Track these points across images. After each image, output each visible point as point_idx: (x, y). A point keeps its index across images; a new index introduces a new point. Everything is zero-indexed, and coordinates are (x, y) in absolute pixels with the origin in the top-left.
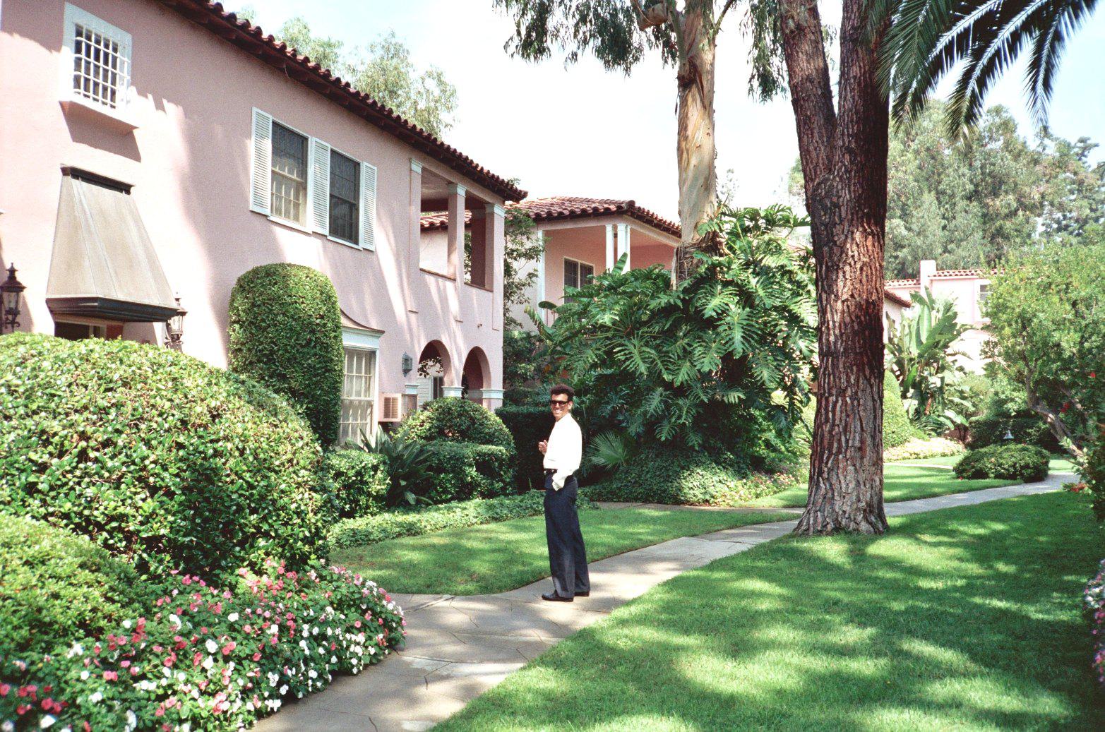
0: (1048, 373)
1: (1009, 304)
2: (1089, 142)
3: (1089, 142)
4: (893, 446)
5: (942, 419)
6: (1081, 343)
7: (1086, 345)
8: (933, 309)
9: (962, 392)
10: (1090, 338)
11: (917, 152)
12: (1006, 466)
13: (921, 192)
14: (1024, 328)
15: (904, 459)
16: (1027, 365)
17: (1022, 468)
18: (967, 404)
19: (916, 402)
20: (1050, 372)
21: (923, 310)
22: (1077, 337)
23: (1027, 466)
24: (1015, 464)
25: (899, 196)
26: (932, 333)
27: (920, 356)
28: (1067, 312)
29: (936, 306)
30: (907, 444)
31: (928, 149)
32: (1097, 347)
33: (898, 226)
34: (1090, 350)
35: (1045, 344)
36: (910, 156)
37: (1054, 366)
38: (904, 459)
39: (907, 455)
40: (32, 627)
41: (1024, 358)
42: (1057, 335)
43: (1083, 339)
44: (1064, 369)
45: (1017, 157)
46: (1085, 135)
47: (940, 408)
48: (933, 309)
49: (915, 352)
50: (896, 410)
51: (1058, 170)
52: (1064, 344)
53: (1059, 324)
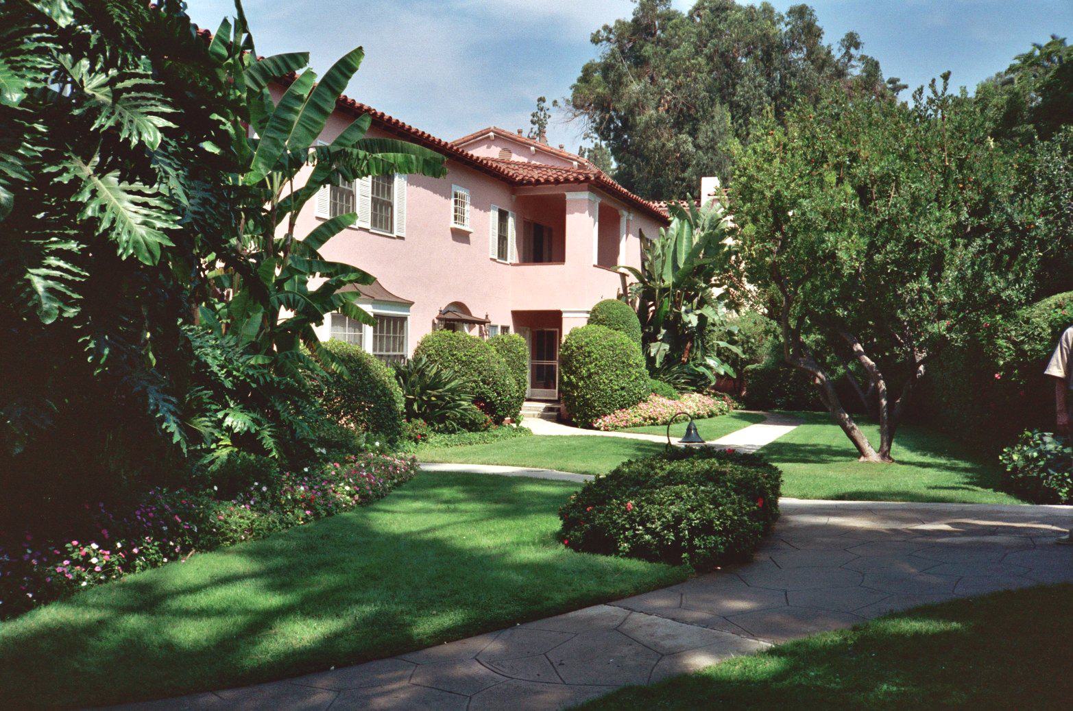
0: (816, 304)
1: (756, 186)
2: (898, 83)
3: (898, 83)
4: (621, 407)
5: (702, 369)
6: (869, 256)
7: (878, 258)
8: (697, 226)
9: (730, 333)
10: (884, 246)
11: (710, 58)
12: (657, 525)
13: (713, 105)
14: (777, 226)
15: (635, 425)
16: (783, 290)
17: (694, 531)
18: (737, 350)
19: (667, 347)
20: (820, 303)
21: (682, 226)
22: (863, 243)
23: (706, 528)
24: (678, 519)
25: (689, 108)
26: (693, 254)
27: (675, 285)
28: (845, 198)
29: (700, 223)
30: (642, 405)
31: (722, 55)
32: (895, 262)
33: (685, 142)
34: (884, 265)
35: (811, 252)
36: (701, 60)
37: (827, 296)
38: (635, 425)
39: (639, 420)
40: (989, 328)
41: (778, 278)
42: (830, 237)
43: (873, 248)
44: (844, 299)
45: (820, 69)
46: (896, 76)
47: (699, 354)
48: (697, 226)
49: (669, 280)
50: (628, 356)
51: (864, 91)
52: (842, 255)
53: (836, 221)
